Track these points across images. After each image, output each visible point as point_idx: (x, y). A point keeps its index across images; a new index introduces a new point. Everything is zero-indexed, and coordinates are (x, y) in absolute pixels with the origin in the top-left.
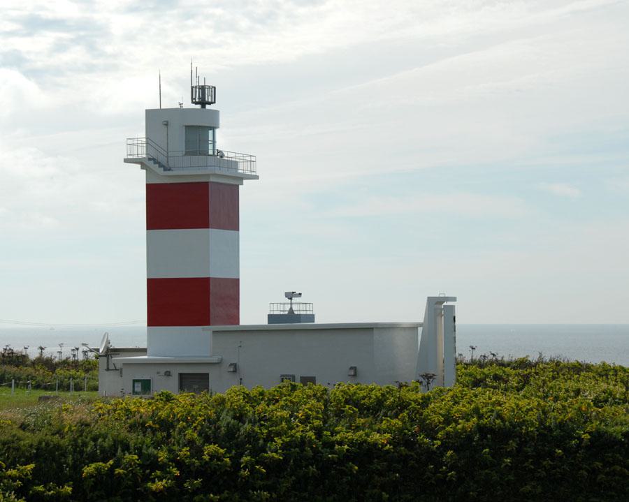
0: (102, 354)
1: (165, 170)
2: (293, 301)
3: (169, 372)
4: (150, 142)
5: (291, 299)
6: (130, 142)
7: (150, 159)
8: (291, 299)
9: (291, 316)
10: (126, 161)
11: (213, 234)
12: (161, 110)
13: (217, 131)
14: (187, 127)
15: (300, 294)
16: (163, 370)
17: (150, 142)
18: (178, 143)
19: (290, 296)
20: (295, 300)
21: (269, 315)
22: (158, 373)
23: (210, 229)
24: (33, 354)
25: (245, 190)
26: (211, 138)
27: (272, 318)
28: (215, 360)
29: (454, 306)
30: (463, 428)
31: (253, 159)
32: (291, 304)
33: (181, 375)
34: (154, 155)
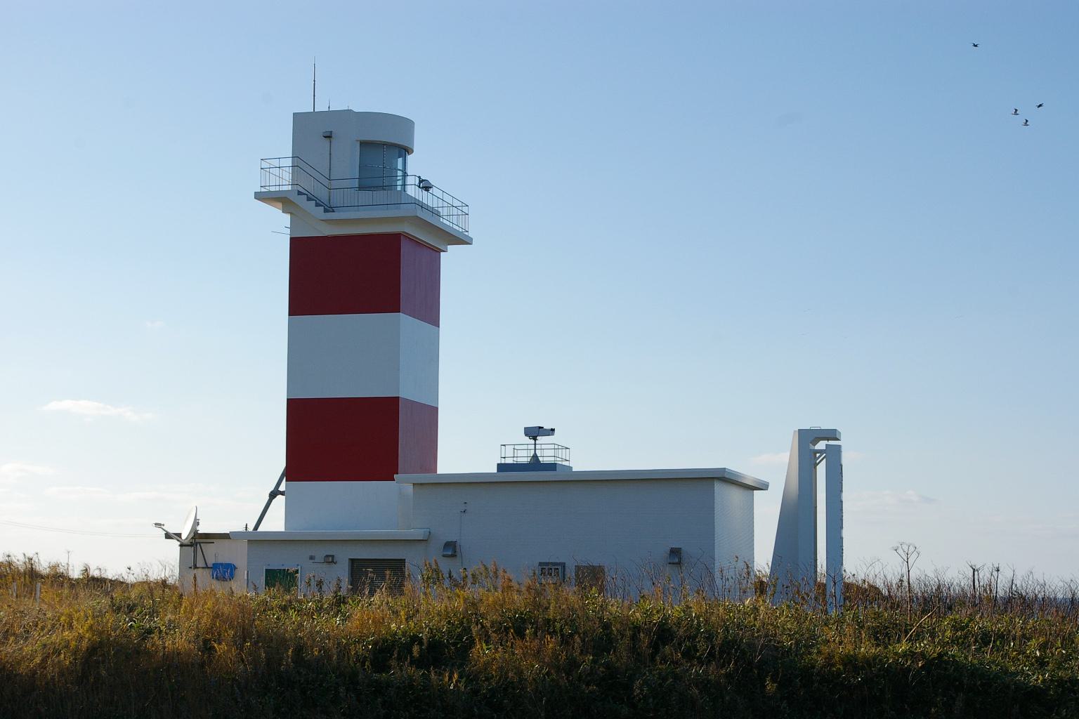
0: (186, 542)
1: (326, 211)
2: (537, 442)
3: (333, 556)
4: (302, 165)
5: (535, 439)
6: (265, 165)
7: (300, 193)
8: (535, 439)
9: (535, 464)
10: (260, 196)
11: (404, 321)
12: (315, 114)
13: (409, 158)
14: (364, 144)
15: (553, 430)
16: (320, 553)
17: (302, 165)
18: (347, 163)
19: (534, 433)
20: (541, 439)
21: (498, 464)
22: (312, 558)
23: (402, 316)
24: (76, 574)
25: (451, 259)
26: (400, 166)
27: (501, 467)
28: (417, 533)
29: (840, 446)
30: (953, 656)
31: (465, 209)
32: (535, 444)
33: (352, 561)
34: (309, 185)
